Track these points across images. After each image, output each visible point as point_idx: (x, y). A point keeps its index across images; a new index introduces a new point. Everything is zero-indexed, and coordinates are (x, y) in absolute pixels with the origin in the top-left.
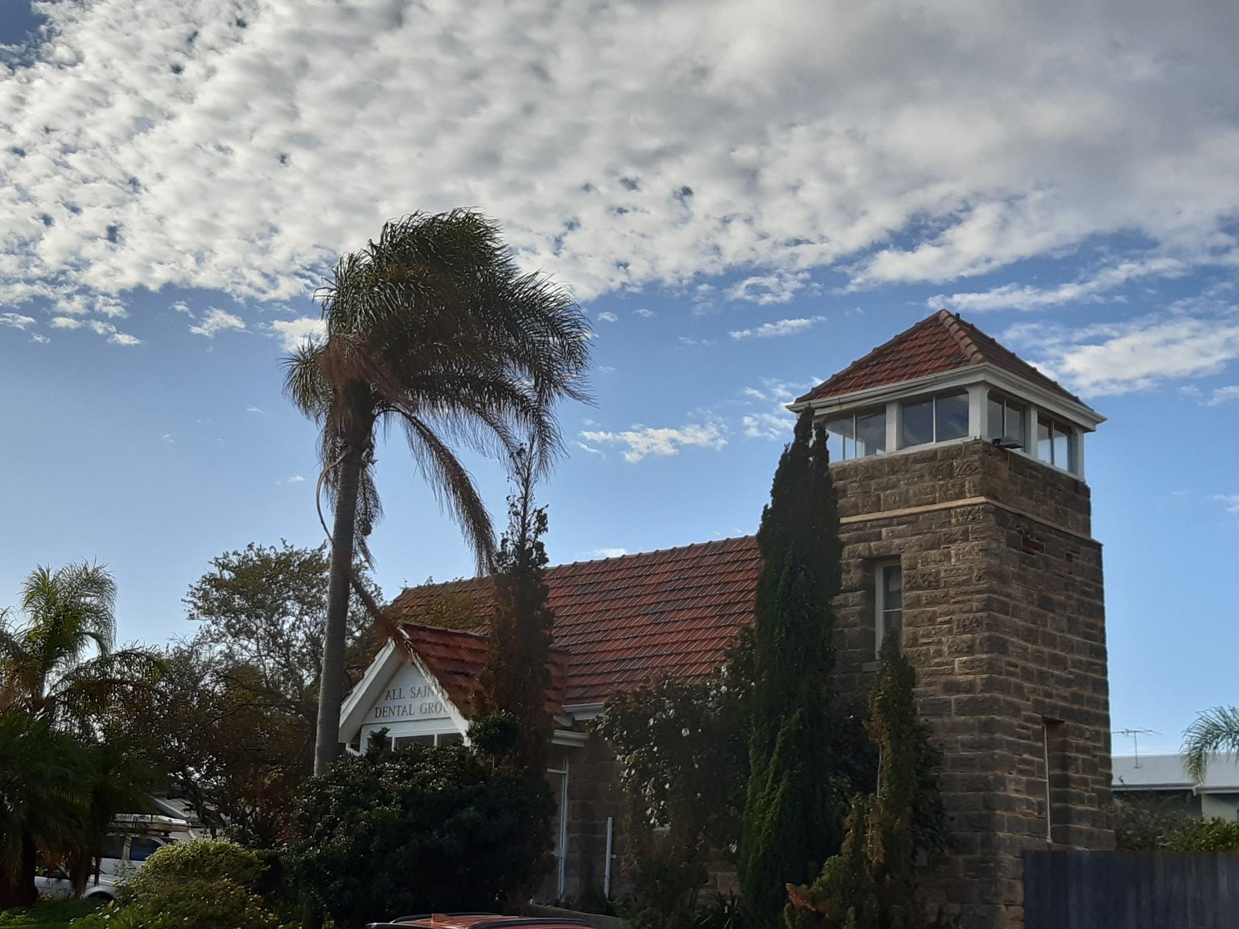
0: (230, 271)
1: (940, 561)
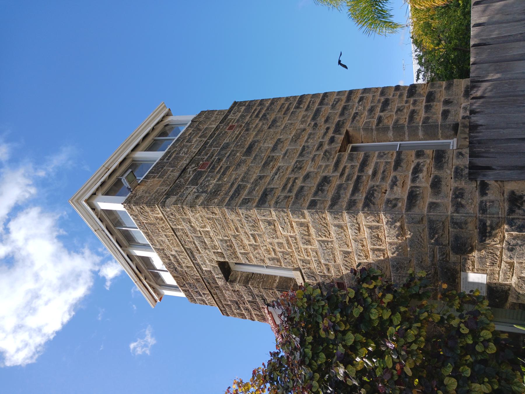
1: (211, 238)
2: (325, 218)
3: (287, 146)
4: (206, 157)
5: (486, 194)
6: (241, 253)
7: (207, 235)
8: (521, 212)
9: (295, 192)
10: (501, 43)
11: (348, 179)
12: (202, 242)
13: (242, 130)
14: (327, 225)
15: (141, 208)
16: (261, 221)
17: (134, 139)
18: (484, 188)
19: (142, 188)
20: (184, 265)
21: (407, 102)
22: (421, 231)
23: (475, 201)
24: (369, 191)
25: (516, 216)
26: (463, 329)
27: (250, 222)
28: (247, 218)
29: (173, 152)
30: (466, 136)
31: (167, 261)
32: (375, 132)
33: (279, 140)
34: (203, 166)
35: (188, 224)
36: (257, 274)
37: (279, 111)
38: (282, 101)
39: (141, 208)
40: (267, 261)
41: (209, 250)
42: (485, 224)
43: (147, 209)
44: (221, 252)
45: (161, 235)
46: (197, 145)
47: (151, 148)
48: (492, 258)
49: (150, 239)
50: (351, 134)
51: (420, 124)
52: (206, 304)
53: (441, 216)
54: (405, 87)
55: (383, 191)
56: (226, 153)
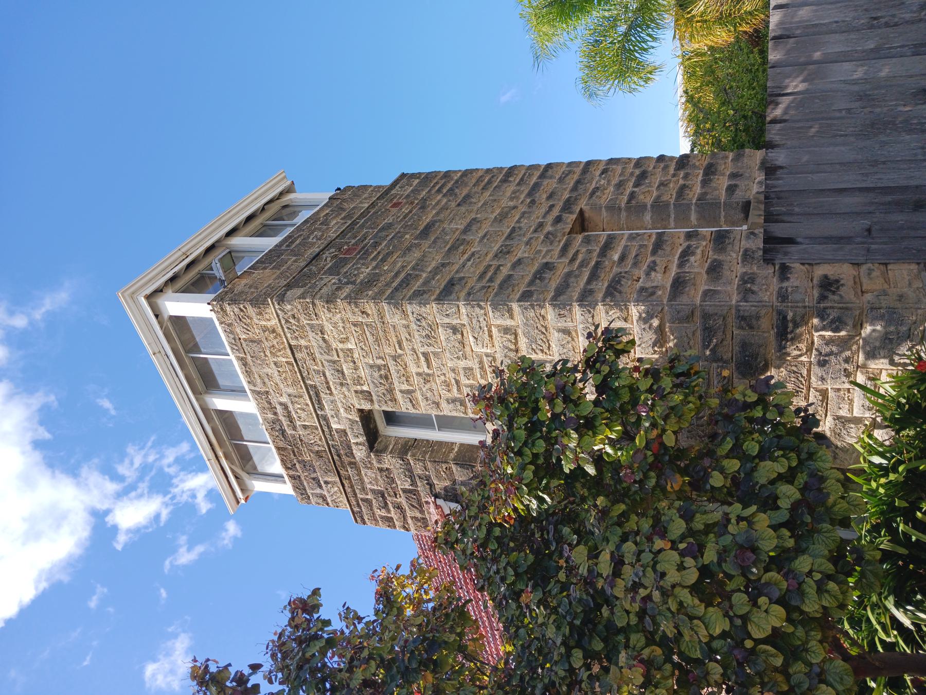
0: (588, 587)
1: (355, 363)
2: (543, 317)
3: (486, 227)
4: (353, 241)
5: (788, 279)
6: (401, 391)
7: (348, 356)
8: (836, 298)
9: (499, 282)
10: (811, 35)
11: (582, 265)
12: (338, 371)
13: (415, 207)
14: (546, 331)
15: (240, 309)
16: (442, 326)
17: (232, 217)
18: (784, 272)
19: (244, 282)
20: (298, 423)
21: (674, 175)
22: (690, 335)
23: (771, 288)
24: (614, 278)
25: (829, 305)
26: (750, 397)
27: (424, 328)
28: (418, 320)
29: (298, 237)
30: (762, 213)
31: (270, 416)
32: (624, 214)
33: (474, 219)
34: (348, 251)
35: (319, 338)
36: (423, 440)
37: (474, 185)
38: (480, 174)
39: (240, 309)
40: (444, 405)
41: (348, 388)
42: (785, 318)
43: (251, 311)
44: (367, 392)
45: (268, 362)
46: (339, 228)
47: (262, 233)
48: (796, 380)
49: (247, 372)
50: (587, 215)
51: (694, 201)
52: (328, 504)
53: (720, 306)
54: (672, 158)
55: (635, 278)
56: (387, 236)
